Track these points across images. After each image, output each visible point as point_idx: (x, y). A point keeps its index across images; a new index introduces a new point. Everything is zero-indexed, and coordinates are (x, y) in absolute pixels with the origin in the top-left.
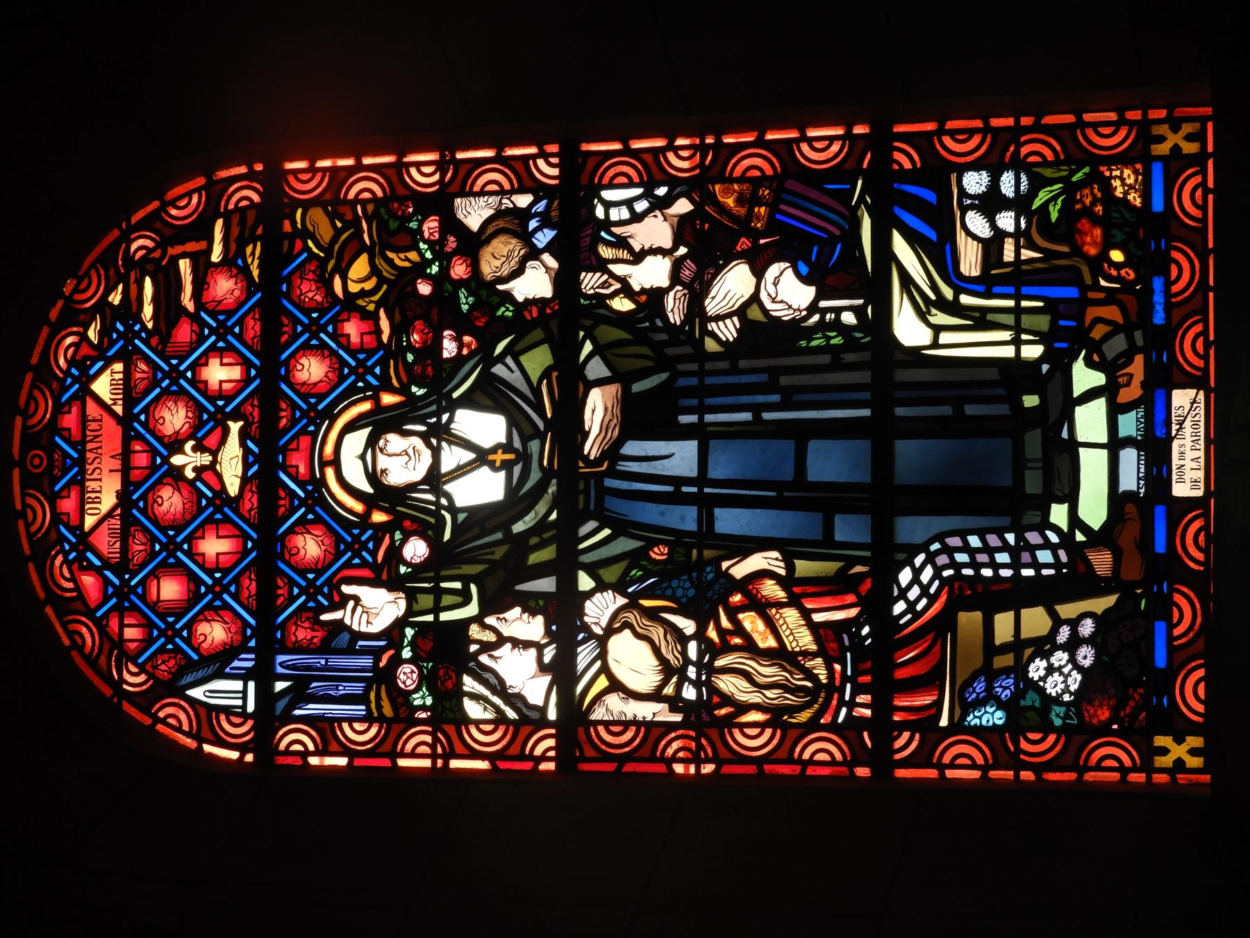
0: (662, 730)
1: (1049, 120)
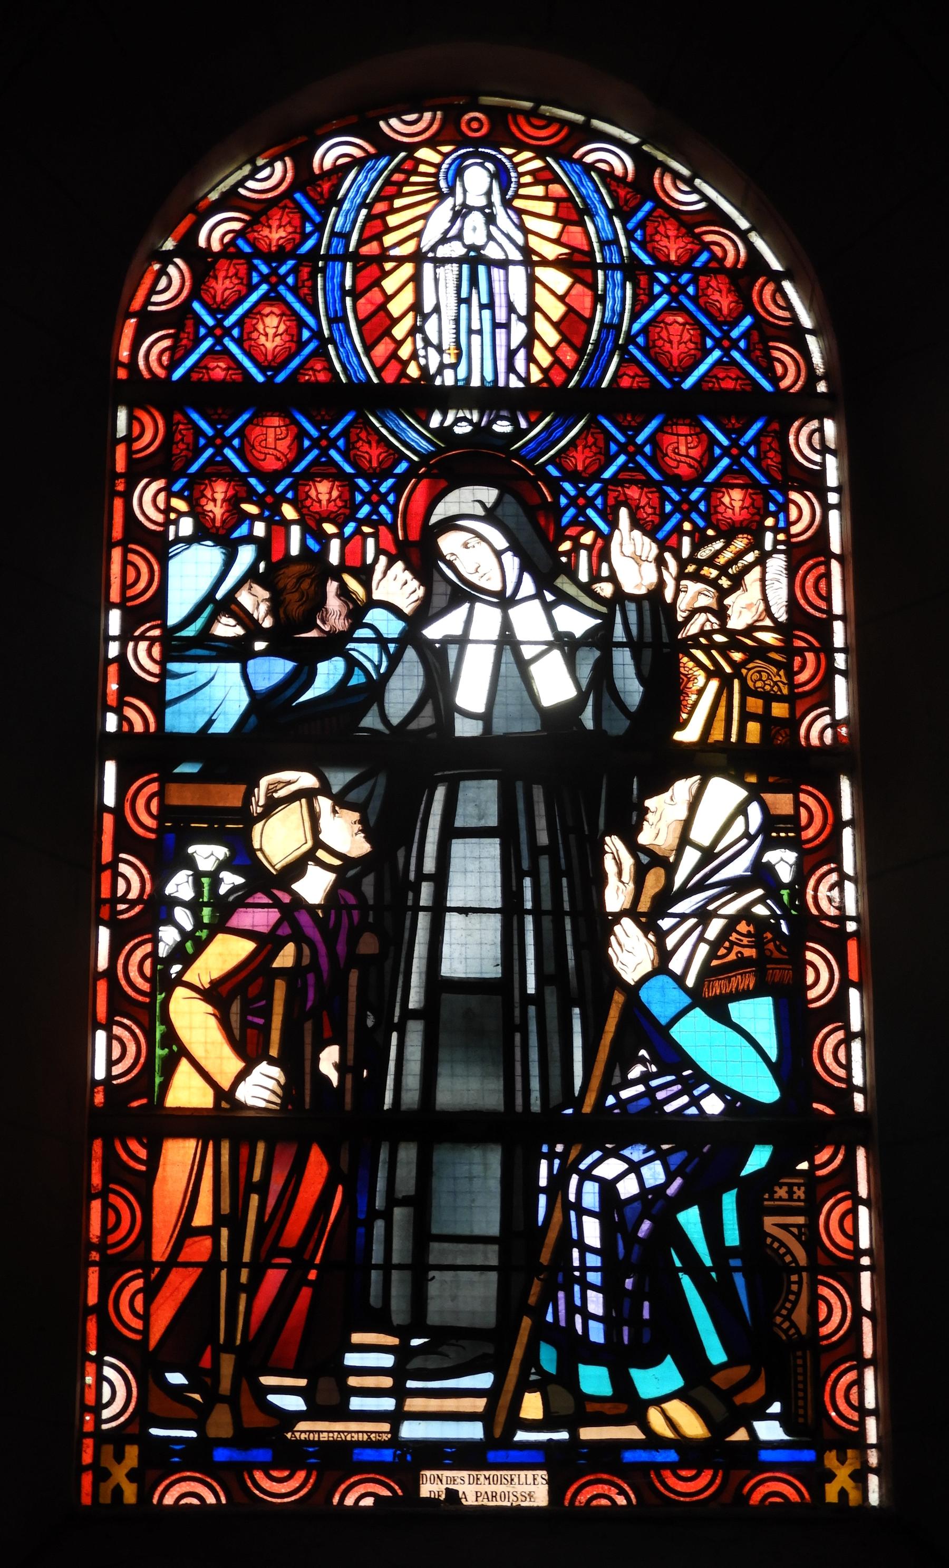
0: (146, 1024)
1: (867, 1324)
